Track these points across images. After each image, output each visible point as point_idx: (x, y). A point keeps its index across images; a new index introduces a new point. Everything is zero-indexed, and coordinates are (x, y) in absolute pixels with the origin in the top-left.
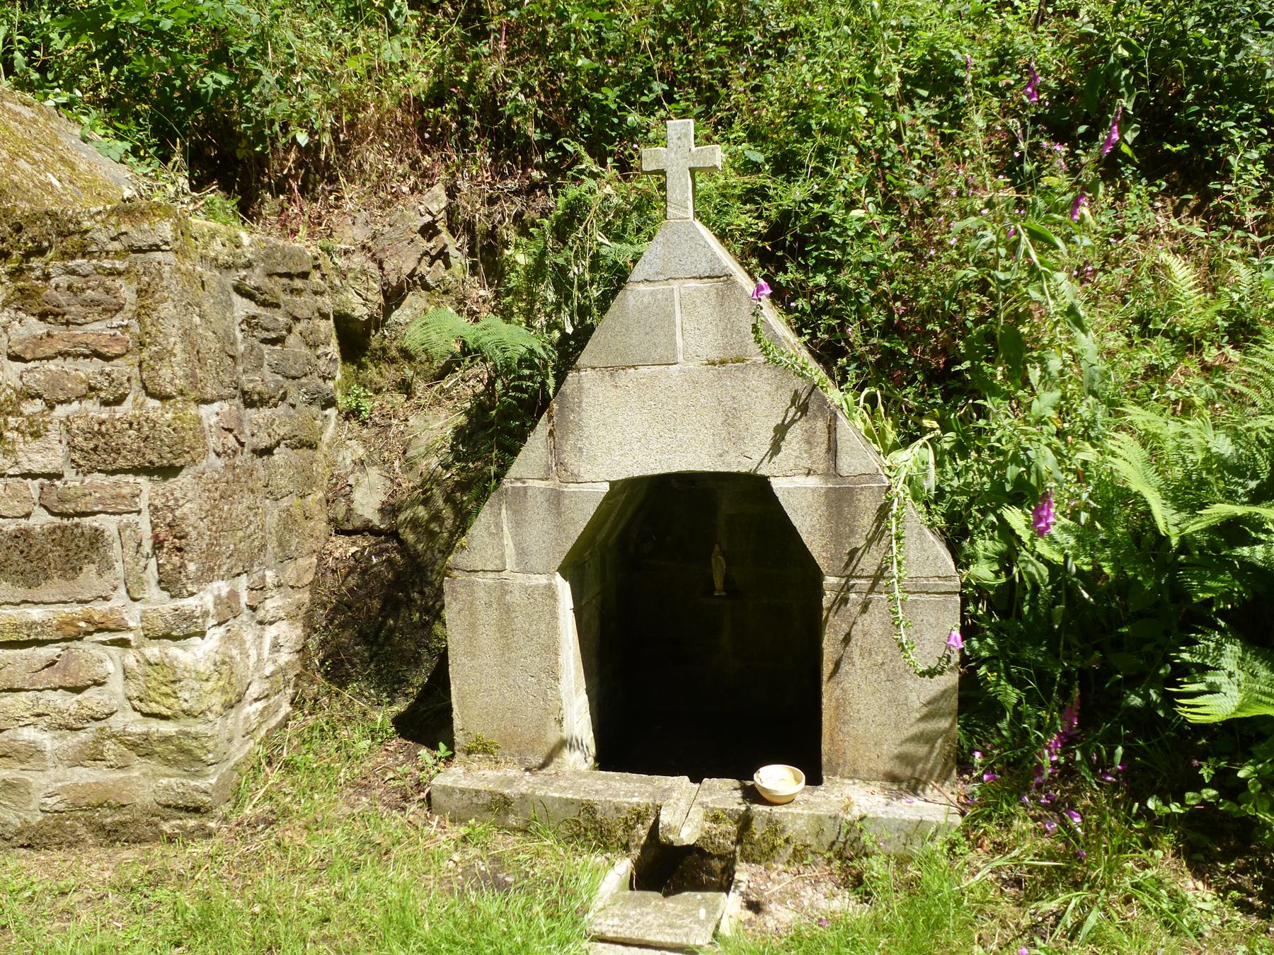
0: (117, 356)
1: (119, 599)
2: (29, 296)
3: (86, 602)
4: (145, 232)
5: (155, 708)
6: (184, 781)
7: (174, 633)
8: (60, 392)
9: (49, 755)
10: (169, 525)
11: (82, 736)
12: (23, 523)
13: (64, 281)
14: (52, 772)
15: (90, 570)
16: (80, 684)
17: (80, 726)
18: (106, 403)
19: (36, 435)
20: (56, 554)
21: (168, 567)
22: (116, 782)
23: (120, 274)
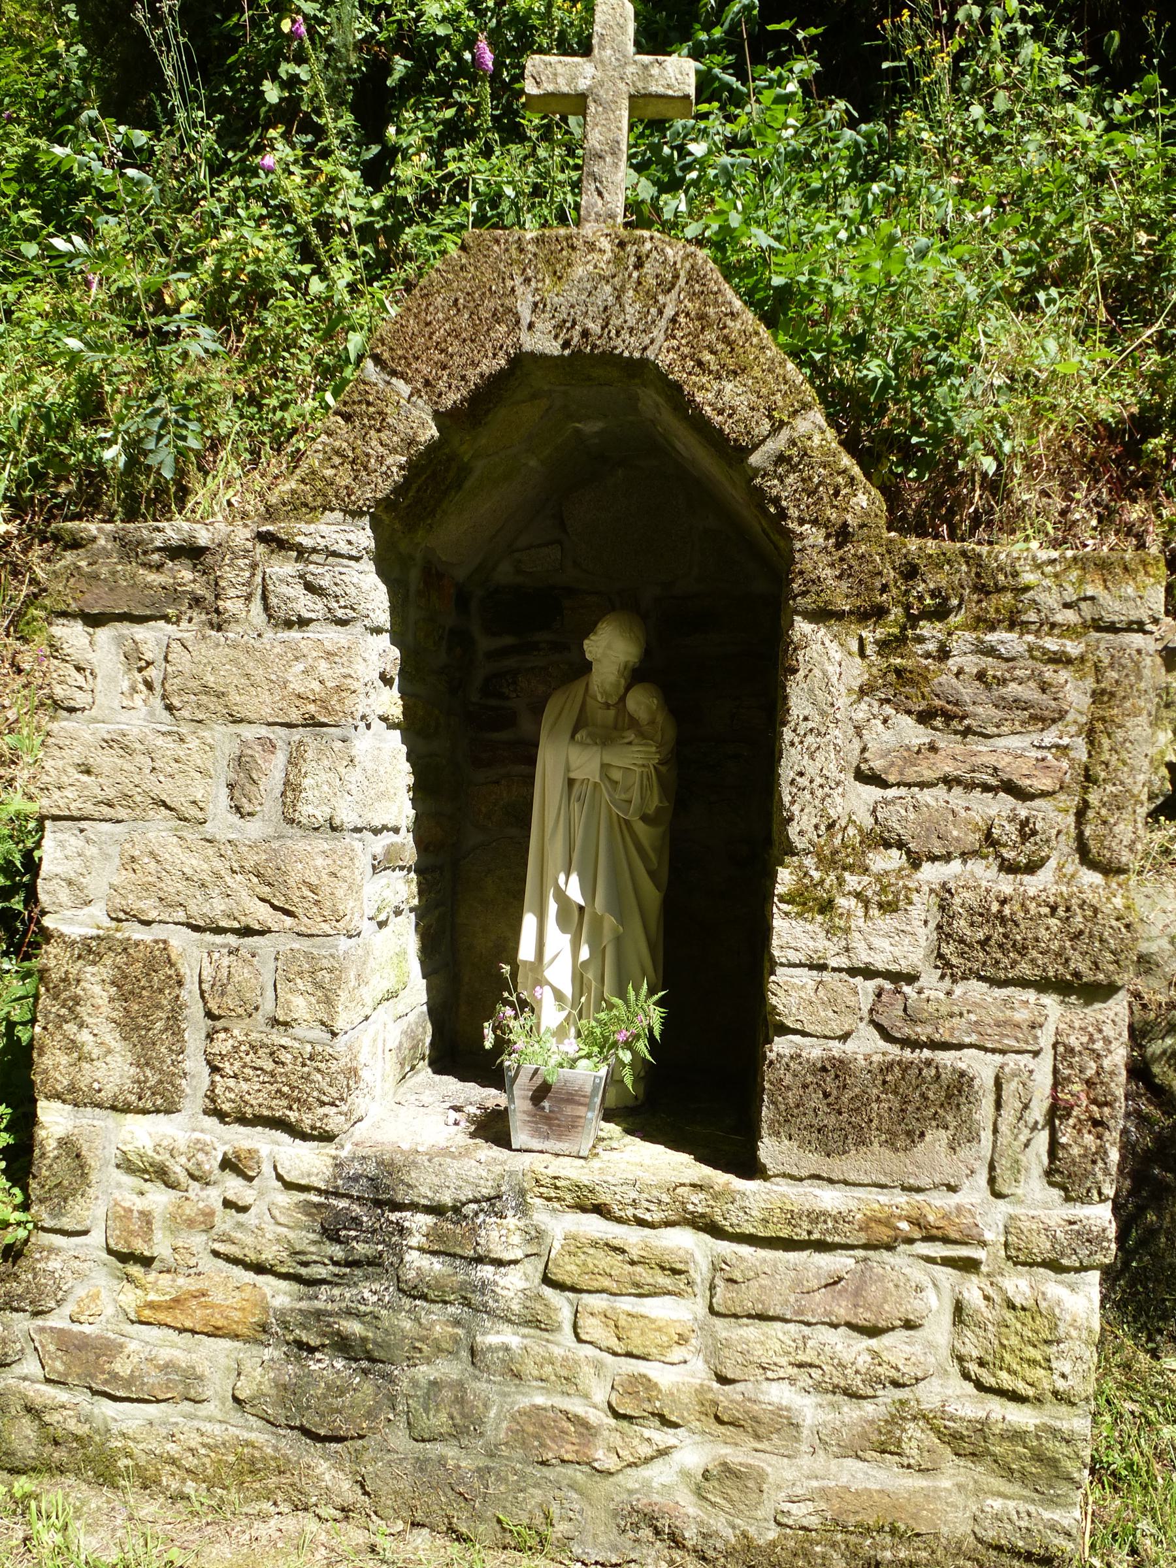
0: (1044, 794)
1: (974, 1193)
2: (912, 683)
3: (919, 1190)
4: (1127, 599)
5: (1006, 1381)
6: (1032, 1509)
7: (1065, 1262)
8: (937, 843)
9: (806, 1432)
10: (1089, 1083)
11: (869, 1408)
12: (836, 1048)
13: (972, 663)
14: (805, 1461)
15: (938, 1139)
16: (882, 1324)
17: (870, 1392)
18: (1009, 868)
19: (889, 908)
20: (883, 1106)
21: (1076, 1151)
22: (913, 1493)
23: (1069, 661)
